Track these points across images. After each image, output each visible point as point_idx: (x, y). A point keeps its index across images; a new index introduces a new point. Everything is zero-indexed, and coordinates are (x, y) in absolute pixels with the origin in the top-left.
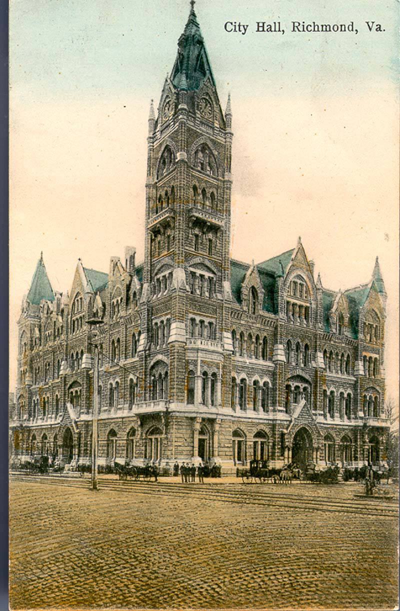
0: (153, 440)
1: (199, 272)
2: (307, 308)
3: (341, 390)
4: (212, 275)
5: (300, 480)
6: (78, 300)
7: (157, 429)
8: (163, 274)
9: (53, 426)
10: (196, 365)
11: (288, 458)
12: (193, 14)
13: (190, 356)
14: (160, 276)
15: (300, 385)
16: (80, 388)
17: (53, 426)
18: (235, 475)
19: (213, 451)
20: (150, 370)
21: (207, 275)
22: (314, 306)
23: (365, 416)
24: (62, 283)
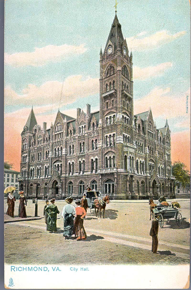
0: (71, 186)
2: (152, 134)
3: (161, 166)
4: (129, 118)
5: (43, 200)
6: (58, 126)
7: (71, 182)
8: (110, 116)
9: (43, 180)
10: (127, 153)
11: (50, 192)
12: (116, 16)
13: (125, 149)
15: (151, 163)
16: (61, 163)
17: (43, 180)
18: (139, 199)
19: (132, 189)
20: (104, 155)
21: (127, 117)
22: (154, 133)
23: (169, 175)
24: (46, 119)
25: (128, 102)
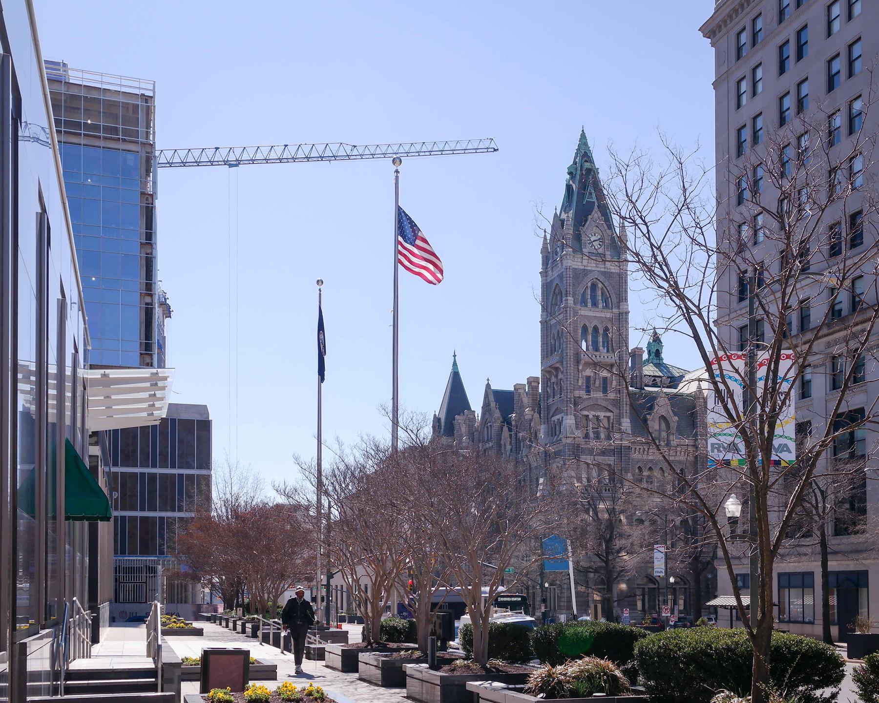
1: (591, 414)
14: (555, 418)
21: (602, 414)
25: (605, 374)
